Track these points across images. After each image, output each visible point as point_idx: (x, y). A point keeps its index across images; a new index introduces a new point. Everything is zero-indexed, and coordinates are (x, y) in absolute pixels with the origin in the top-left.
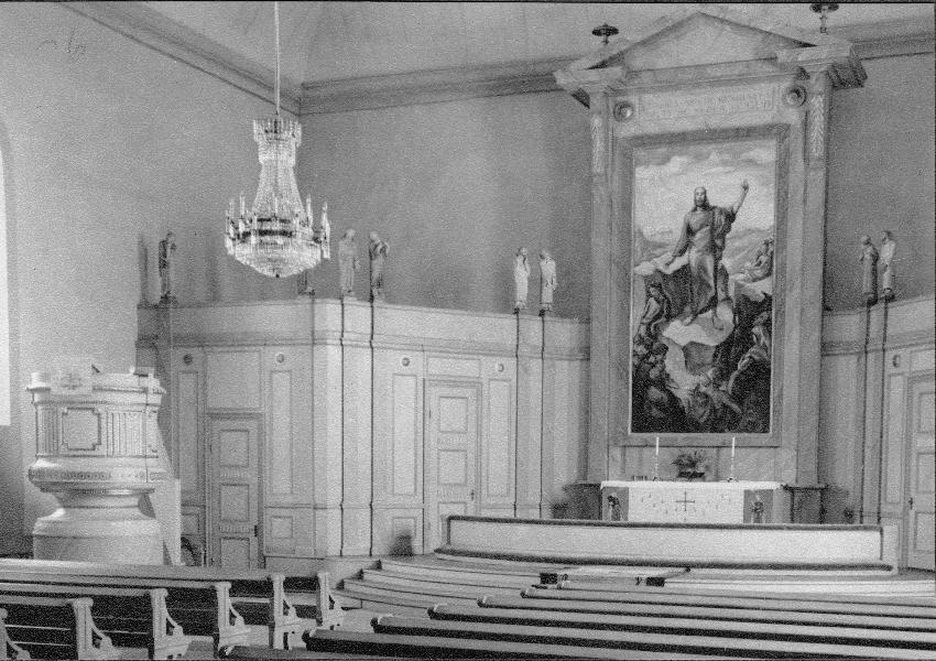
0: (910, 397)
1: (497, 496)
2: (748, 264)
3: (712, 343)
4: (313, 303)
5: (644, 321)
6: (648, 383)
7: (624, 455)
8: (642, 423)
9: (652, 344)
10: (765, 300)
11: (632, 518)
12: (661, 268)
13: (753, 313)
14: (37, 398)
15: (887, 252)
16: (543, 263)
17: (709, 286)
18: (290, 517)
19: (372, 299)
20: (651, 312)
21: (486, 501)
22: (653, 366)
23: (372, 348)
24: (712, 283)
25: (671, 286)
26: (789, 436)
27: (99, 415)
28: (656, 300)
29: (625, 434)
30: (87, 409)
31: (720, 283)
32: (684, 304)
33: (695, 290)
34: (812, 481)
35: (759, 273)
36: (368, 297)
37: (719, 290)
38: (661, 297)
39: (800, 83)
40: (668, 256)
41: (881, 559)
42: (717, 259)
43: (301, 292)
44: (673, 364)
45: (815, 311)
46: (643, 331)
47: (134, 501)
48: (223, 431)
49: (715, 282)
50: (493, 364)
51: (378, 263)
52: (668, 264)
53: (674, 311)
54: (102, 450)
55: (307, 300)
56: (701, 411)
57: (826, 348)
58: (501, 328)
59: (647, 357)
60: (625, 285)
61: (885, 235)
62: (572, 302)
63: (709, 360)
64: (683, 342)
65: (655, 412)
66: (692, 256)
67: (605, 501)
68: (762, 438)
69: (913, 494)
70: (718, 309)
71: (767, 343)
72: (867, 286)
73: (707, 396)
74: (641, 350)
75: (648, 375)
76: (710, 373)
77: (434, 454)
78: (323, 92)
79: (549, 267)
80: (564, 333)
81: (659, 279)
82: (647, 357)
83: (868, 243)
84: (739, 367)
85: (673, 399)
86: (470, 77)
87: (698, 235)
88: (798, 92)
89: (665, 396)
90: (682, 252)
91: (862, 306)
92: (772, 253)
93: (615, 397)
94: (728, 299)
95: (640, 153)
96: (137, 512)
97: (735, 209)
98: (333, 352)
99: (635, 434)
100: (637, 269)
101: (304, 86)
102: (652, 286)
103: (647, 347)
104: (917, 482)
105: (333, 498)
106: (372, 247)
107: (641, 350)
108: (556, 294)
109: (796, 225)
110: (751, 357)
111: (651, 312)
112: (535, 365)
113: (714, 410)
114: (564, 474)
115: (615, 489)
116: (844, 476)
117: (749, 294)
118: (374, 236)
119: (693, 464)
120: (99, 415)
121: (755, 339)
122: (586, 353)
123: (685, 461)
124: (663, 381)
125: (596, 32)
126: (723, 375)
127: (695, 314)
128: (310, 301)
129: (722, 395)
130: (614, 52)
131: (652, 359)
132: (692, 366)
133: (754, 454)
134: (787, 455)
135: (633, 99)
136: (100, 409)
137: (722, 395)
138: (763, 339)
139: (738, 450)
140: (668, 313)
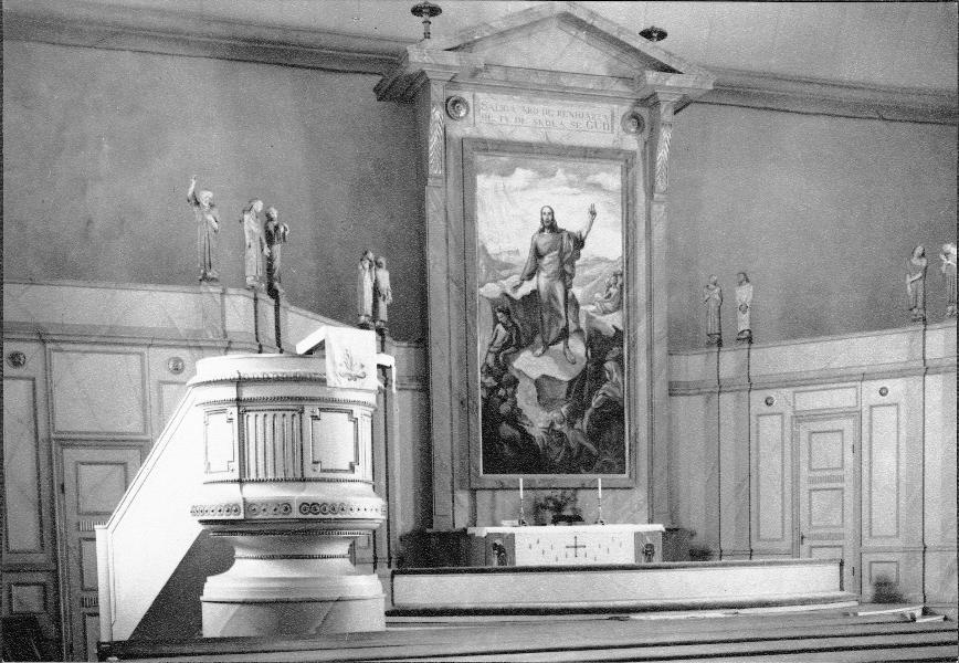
2: (597, 295)
3: (566, 378)
4: (223, 294)
11: (520, 562)
12: (509, 291)
13: (603, 346)
17: (559, 316)
20: (499, 339)
22: (504, 400)
24: (563, 312)
28: (504, 326)
31: (570, 314)
32: (535, 334)
33: (546, 317)
35: (609, 305)
37: (570, 321)
39: (638, 110)
40: (515, 279)
44: (525, 398)
45: (660, 352)
46: (491, 359)
49: (566, 312)
52: (516, 288)
53: (523, 340)
56: (557, 450)
59: (496, 388)
61: (742, 277)
63: (563, 396)
64: (535, 375)
66: (541, 281)
70: (571, 341)
71: (620, 380)
73: (561, 434)
74: (490, 381)
76: (564, 409)
81: (507, 304)
82: (496, 388)
84: (593, 404)
87: (547, 259)
89: (517, 433)
90: (530, 276)
92: (621, 286)
93: (454, 434)
94: (579, 331)
95: (481, 159)
97: (583, 235)
100: (482, 290)
103: (498, 378)
106: (271, 228)
107: (490, 381)
110: (604, 394)
111: (499, 339)
115: (499, 535)
116: (694, 519)
117: (599, 327)
118: (274, 214)
119: (559, 507)
124: (515, 418)
125: (417, 11)
126: (576, 413)
127: (547, 345)
129: (576, 435)
132: (545, 402)
135: (466, 95)
137: (576, 435)
138: (615, 375)
140: (517, 341)
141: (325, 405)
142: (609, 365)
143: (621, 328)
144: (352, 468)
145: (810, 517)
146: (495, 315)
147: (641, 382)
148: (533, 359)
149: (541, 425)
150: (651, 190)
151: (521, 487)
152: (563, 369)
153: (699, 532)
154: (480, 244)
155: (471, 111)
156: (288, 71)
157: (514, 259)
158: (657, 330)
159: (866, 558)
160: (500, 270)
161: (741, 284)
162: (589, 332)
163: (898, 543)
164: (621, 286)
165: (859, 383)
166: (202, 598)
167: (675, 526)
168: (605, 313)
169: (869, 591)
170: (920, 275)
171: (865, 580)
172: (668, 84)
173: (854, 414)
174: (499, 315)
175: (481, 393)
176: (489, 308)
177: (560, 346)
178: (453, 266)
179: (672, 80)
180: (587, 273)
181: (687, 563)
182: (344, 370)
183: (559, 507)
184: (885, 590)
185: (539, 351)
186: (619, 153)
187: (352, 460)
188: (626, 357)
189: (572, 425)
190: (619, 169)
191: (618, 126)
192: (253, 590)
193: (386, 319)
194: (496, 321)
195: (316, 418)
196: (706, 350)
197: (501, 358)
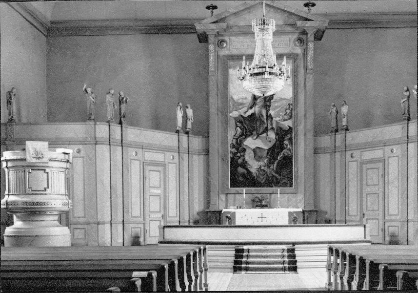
0: (361, 171)
1: (174, 220)
2: (281, 114)
3: (266, 148)
4: (95, 124)
5: (235, 137)
6: (237, 165)
7: (226, 198)
8: (235, 183)
9: (239, 147)
10: (289, 129)
11: (237, 224)
13: (284, 134)
14: (10, 164)
15: (344, 110)
16: (187, 110)
17: (263, 122)
18: (84, 229)
19: (121, 123)
20: (238, 133)
21: (168, 219)
22: (239, 157)
23: (110, 145)
24: (265, 121)
25: (247, 122)
26: (301, 188)
27: (47, 173)
28: (240, 128)
29: (227, 188)
30: (42, 170)
31: (269, 122)
34: (312, 208)
35: (286, 117)
36: (118, 122)
37: (269, 125)
38: (243, 127)
39: (301, 36)
40: (245, 109)
41: (365, 238)
42: (267, 111)
43: (89, 119)
44: (249, 157)
45: (310, 135)
47: (56, 218)
48: (368, 169)
49: (267, 121)
50: (169, 155)
51: (123, 106)
52: (245, 112)
53: (248, 133)
54: (48, 191)
55: (92, 123)
56: (262, 177)
57: (316, 151)
58: (168, 139)
60: (225, 122)
61: (343, 102)
62: (203, 130)
63: (265, 155)
64: (253, 147)
65: (241, 179)
66: (256, 109)
67: (224, 218)
68: (287, 189)
69: (365, 211)
70: (269, 133)
71: (290, 148)
72: (333, 124)
73: (264, 171)
74: (234, 150)
75: (237, 162)
76: (265, 161)
77: (148, 198)
78: (61, 26)
79: (190, 112)
80: (197, 142)
82: (237, 153)
83: (334, 106)
84: (279, 158)
85: (249, 172)
86: (139, 23)
88: (300, 40)
89: (245, 171)
90: (251, 108)
91: (332, 132)
92: (292, 109)
93: (221, 171)
94: (273, 128)
95: (231, 63)
96: (57, 223)
98: (106, 148)
99: (232, 188)
100: (230, 114)
101: (52, 23)
102: (238, 122)
103: (237, 149)
104: (367, 206)
105: (108, 218)
106: (121, 99)
107: (234, 150)
108: (192, 124)
109: (301, 97)
110: (283, 154)
111: (238, 133)
112: (186, 156)
113: (268, 178)
114: (198, 206)
115: (229, 212)
116: (325, 205)
117: (281, 126)
118: (122, 93)
119: (261, 201)
120: (47, 173)
121: (285, 146)
122: (207, 153)
123: (257, 200)
124: (244, 165)
125: (208, 8)
126: (271, 162)
127: (258, 135)
128: (94, 123)
129: (271, 171)
130: (223, 16)
131: (239, 155)
132: (257, 157)
133: (286, 196)
134: (300, 196)
135: (226, 38)
136: (47, 170)
137: (271, 171)
138: (289, 146)
139: (281, 194)
140: (245, 134)
141: (33, 168)
142: (286, 142)
143: (291, 126)
144: (45, 190)
145: (367, 206)
146: (236, 123)
147: (301, 150)
148: (253, 141)
149: (255, 167)
150: (306, 68)
151: (279, 193)
152: (266, 145)
153: (329, 212)
154: (230, 96)
155: (229, 45)
156: (167, 35)
157: (245, 101)
158: (308, 127)
159: (387, 224)
160: (239, 106)
161: (343, 105)
162: (277, 128)
163: (398, 218)
164: (292, 109)
165: (384, 147)
166: (4, 235)
167: (316, 209)
168: (285, 120)
169: (388, 238)
170: (406, 99)
171: (387, 233)
172: (307, 25)
173: (383, 161)
174: (238, 123)
175: (229, 155)
176: (234, 121)
177: (265, 135)
178: (220, 105)
179: (308, 24)
180: (276, 105)
181: (323, 225)
182: (34, 156)
183: (261, 201)
184: (394, 239)
185: (255, 137)
186: (291, 55)
187: (46, 186)
188: (293, 138)
189: (269, 167)
190: (291, 61)
191: (292, 44)
192: (14, 232)
193: (181, 126)
194: (237, 126)
195: (29, 172)
196: (330, 134)
197: (238, 141)
